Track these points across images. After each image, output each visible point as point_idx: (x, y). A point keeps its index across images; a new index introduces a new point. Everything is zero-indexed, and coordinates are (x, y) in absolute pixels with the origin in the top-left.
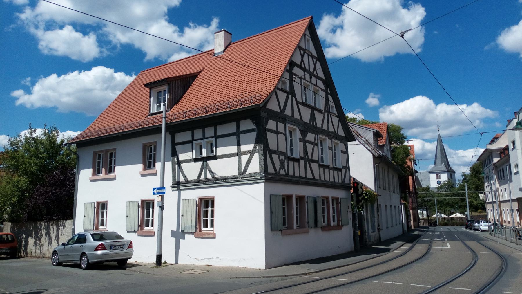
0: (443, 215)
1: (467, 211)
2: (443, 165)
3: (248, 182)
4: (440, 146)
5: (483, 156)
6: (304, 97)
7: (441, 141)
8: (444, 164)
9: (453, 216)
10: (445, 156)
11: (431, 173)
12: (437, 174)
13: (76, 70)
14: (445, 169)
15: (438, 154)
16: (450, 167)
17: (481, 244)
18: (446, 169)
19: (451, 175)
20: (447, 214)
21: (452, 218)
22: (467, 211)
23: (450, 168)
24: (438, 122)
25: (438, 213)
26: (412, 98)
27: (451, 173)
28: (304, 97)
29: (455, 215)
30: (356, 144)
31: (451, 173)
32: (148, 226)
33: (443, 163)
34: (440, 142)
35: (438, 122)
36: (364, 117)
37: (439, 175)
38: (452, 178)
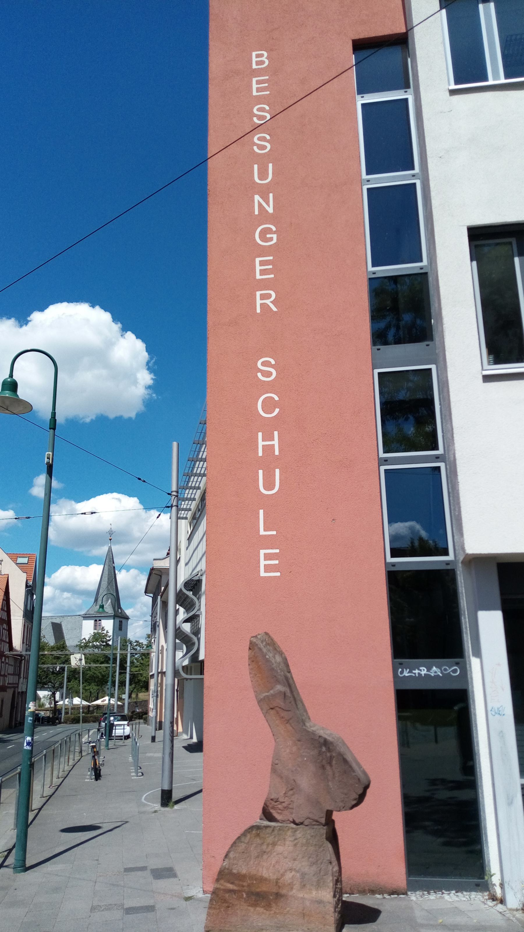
0: (77, 701)
1: (125, 694)
2: (108, 603)
3: (29, 632)
4: (109, 569)
7: (112, 560)
8: (111, 602)
9: (99, 702)
10: (114, 587)
12: (96, 621)
16: (121, 608)
17: (55, 735)
19: (121, 622)
21: (98, 707)
22: (125, 694)
23: (120, 611)
25: (66, 698)
27: (121, 620)
29: (102, 701)
30: (82, 514)
31: (121, 620)
32: (387, 471)
33: (110, 601)
34: (110, 561)
36: (38, 474)
37: (100, 623)
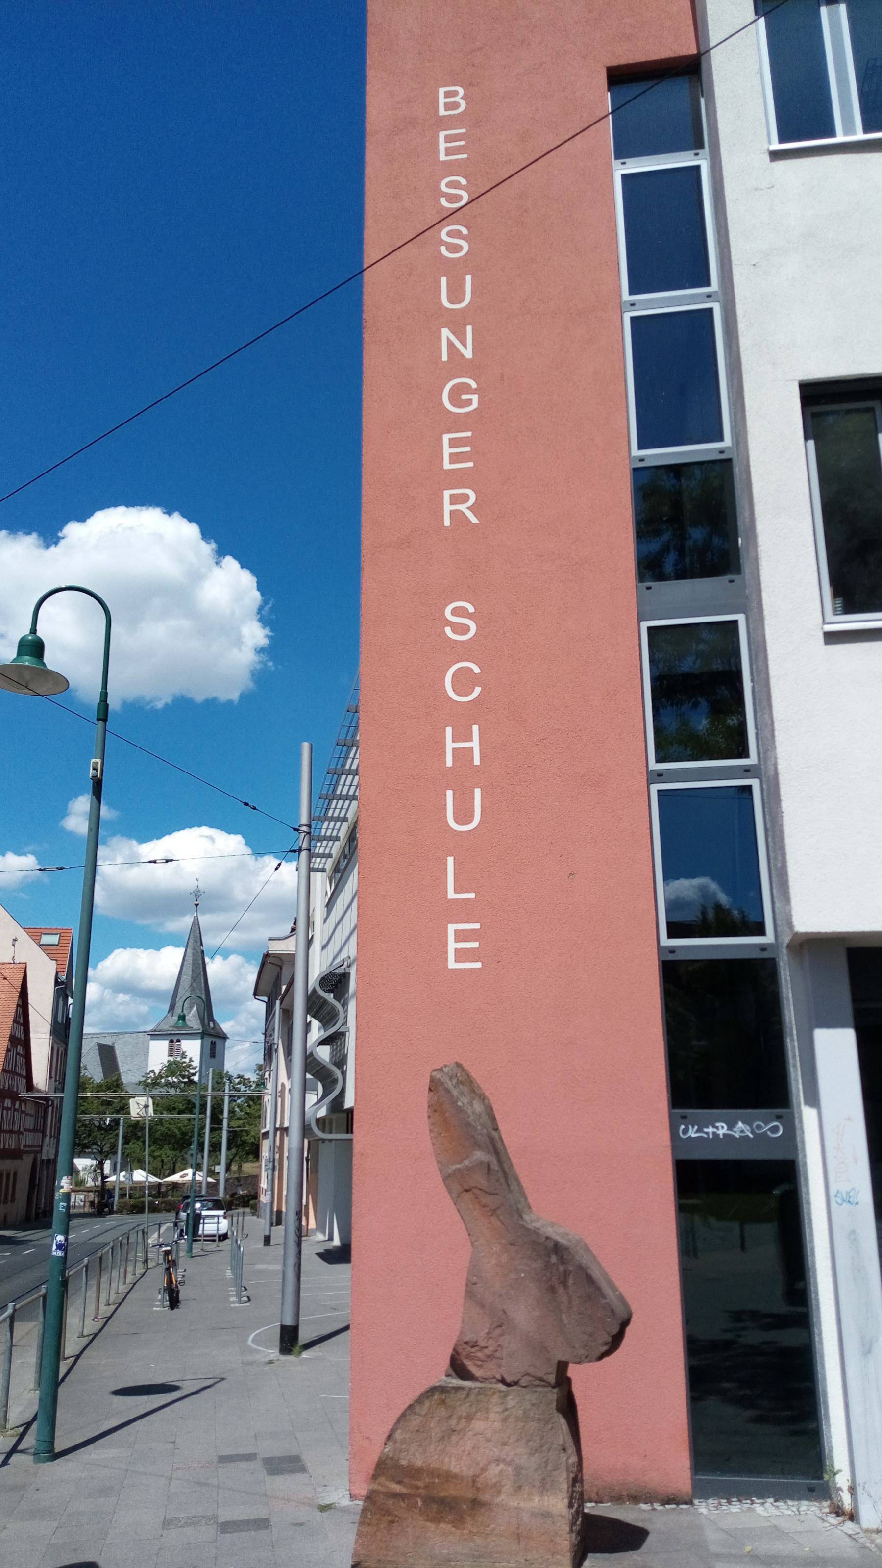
2: (192, 1012)
5: (264, 977)
6: (55, 932)
9: (176, 1178)
10: (203, 985)
11: (155, 1035)
12: (172, 1041)
13: (236, 833)
14: (195, 1027)
15: (183, 978)
18: (201, 1027)
19: (213, 1044)
20: (128, 1151)
23: (211, 1025)
24: (857, 1203)
25: (121, 1171)
26: (170, 834)
27: (214, 1040)
28: (55, 932)
29: (181, 1177)
31: (214, 1040)
33: (195, 1008)
35: (857, 1203)
38: (213, 1055)
